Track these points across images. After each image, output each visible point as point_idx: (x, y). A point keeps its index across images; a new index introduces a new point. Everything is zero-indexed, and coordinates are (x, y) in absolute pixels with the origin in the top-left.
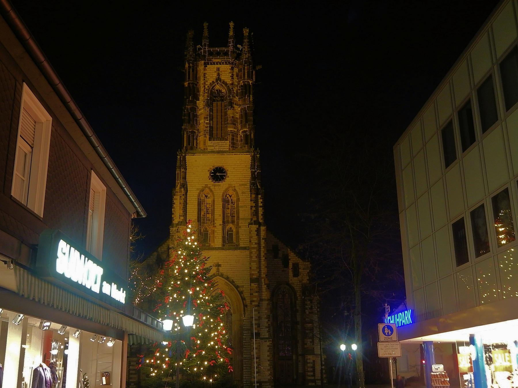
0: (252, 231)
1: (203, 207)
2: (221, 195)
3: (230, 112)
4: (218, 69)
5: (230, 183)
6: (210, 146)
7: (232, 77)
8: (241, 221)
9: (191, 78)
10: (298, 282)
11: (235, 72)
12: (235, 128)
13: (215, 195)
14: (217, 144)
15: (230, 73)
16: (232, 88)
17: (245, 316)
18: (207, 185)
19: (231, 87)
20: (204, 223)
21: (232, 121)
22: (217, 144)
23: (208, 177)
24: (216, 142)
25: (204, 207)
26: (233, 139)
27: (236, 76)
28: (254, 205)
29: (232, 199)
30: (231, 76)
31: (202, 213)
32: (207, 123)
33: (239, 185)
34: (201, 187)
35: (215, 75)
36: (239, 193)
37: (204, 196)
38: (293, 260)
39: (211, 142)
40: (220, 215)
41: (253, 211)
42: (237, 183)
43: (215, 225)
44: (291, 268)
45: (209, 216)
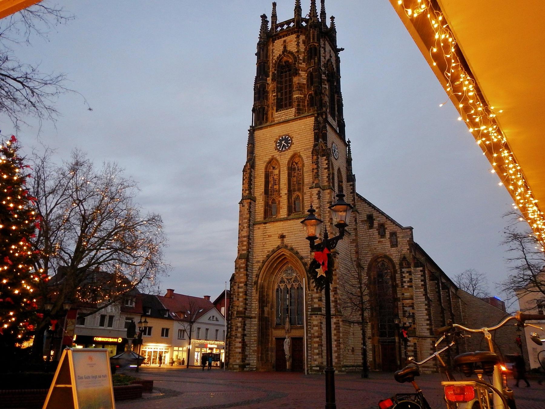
0: (313, 195)
1: (271, 179)
2: (287, 164)
3: (296, 80)
4: (285, 41)
5: (295, 149)
6: (277, 117)
7: (298, 45)
8: (305, 187)
9: (261, 58)
10: (397, 252)
11: (301, 39)
12: (301, 94)
13: (281, 165)
14: (283, 114)
15: (296, 41)
16: (298, 56)
17: (309, 290)
18: (274, 156)
19: (296, 55)
20: (271, 195)
21: (298, 87)
22: (283, 114)
23: (274, 148)
24: (282, 112)
25: (272, 179)
26: (299, 105)
27: (303, 43)
28: (316, 166)
29: (298, 166)
30: (297, 44)
31: (270, 186)
32: (274, 96)
33: (303, 150)
34: (268, 159)
35: (282, 48)
36: (304, 158)
37: (272, 168)
38: (390, 229)
39: (278, 113)
40: (285, 184)
41: (314, 173)
42: (302, 148)
43: (281, 195)
44: (389, 238)
45: (276, 187)
